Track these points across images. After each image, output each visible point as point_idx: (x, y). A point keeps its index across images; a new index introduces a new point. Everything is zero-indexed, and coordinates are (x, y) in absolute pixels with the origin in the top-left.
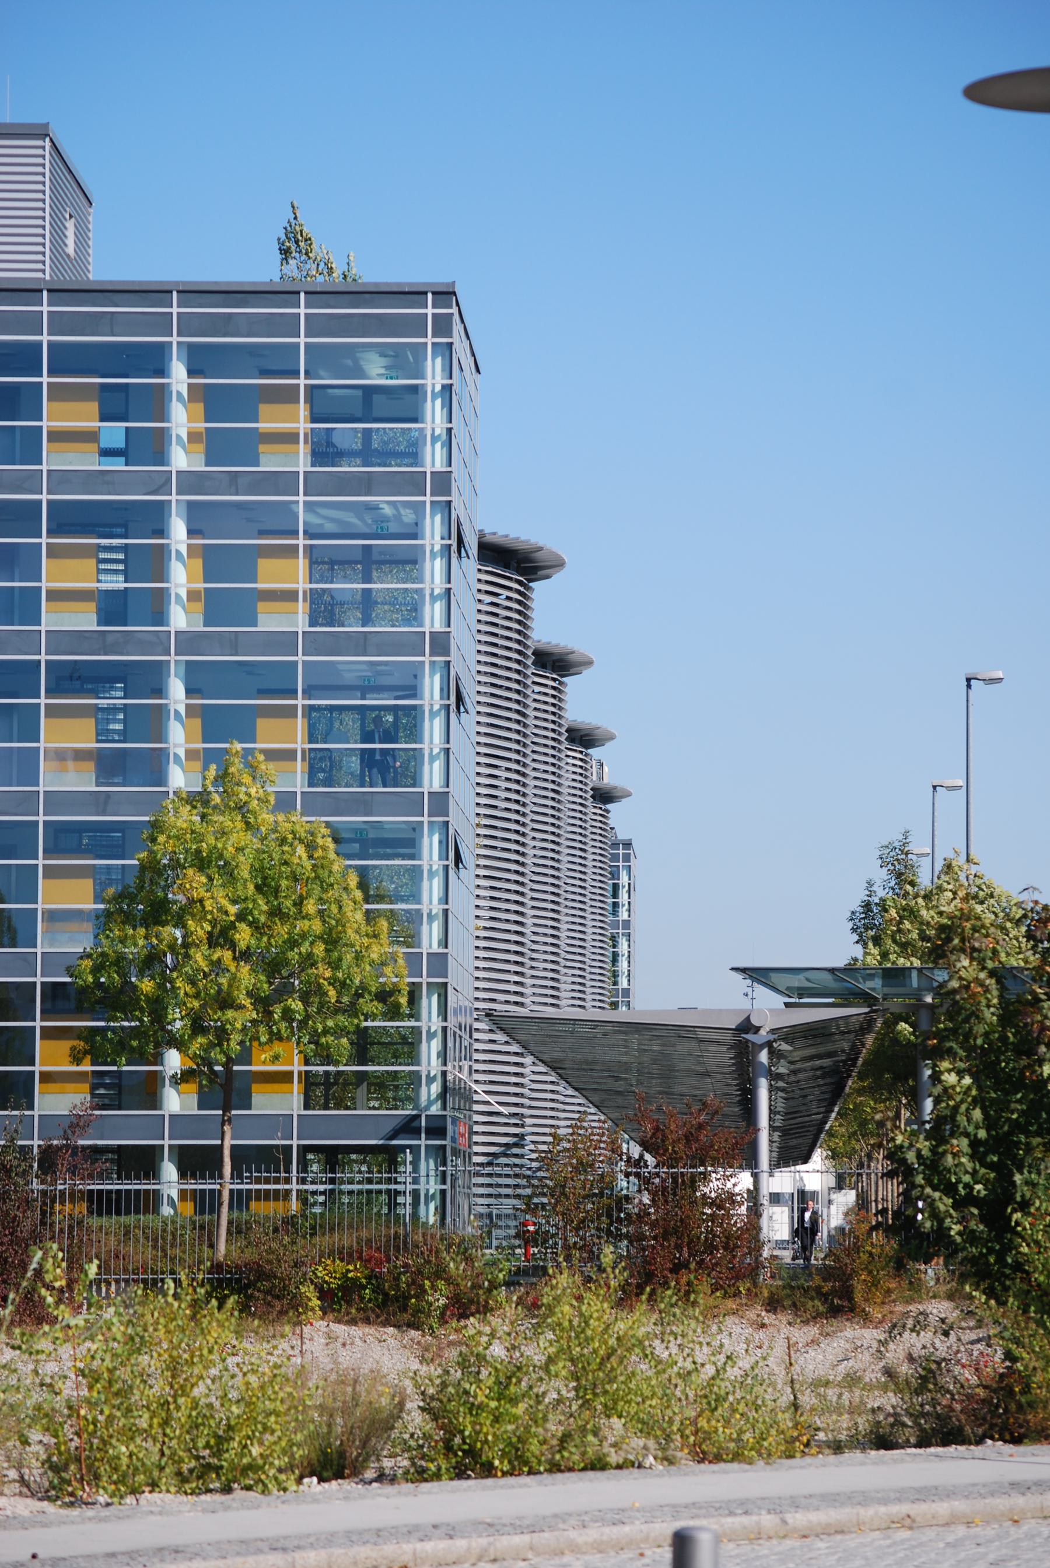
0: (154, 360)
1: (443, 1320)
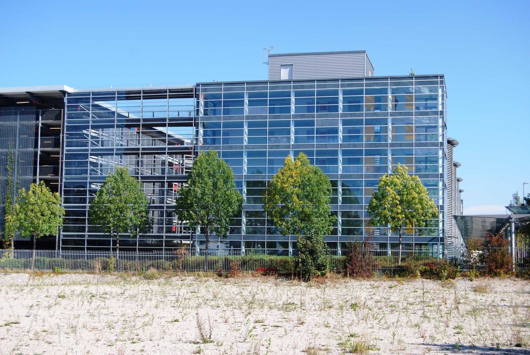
0: (385, 91)
1: (446, 279)
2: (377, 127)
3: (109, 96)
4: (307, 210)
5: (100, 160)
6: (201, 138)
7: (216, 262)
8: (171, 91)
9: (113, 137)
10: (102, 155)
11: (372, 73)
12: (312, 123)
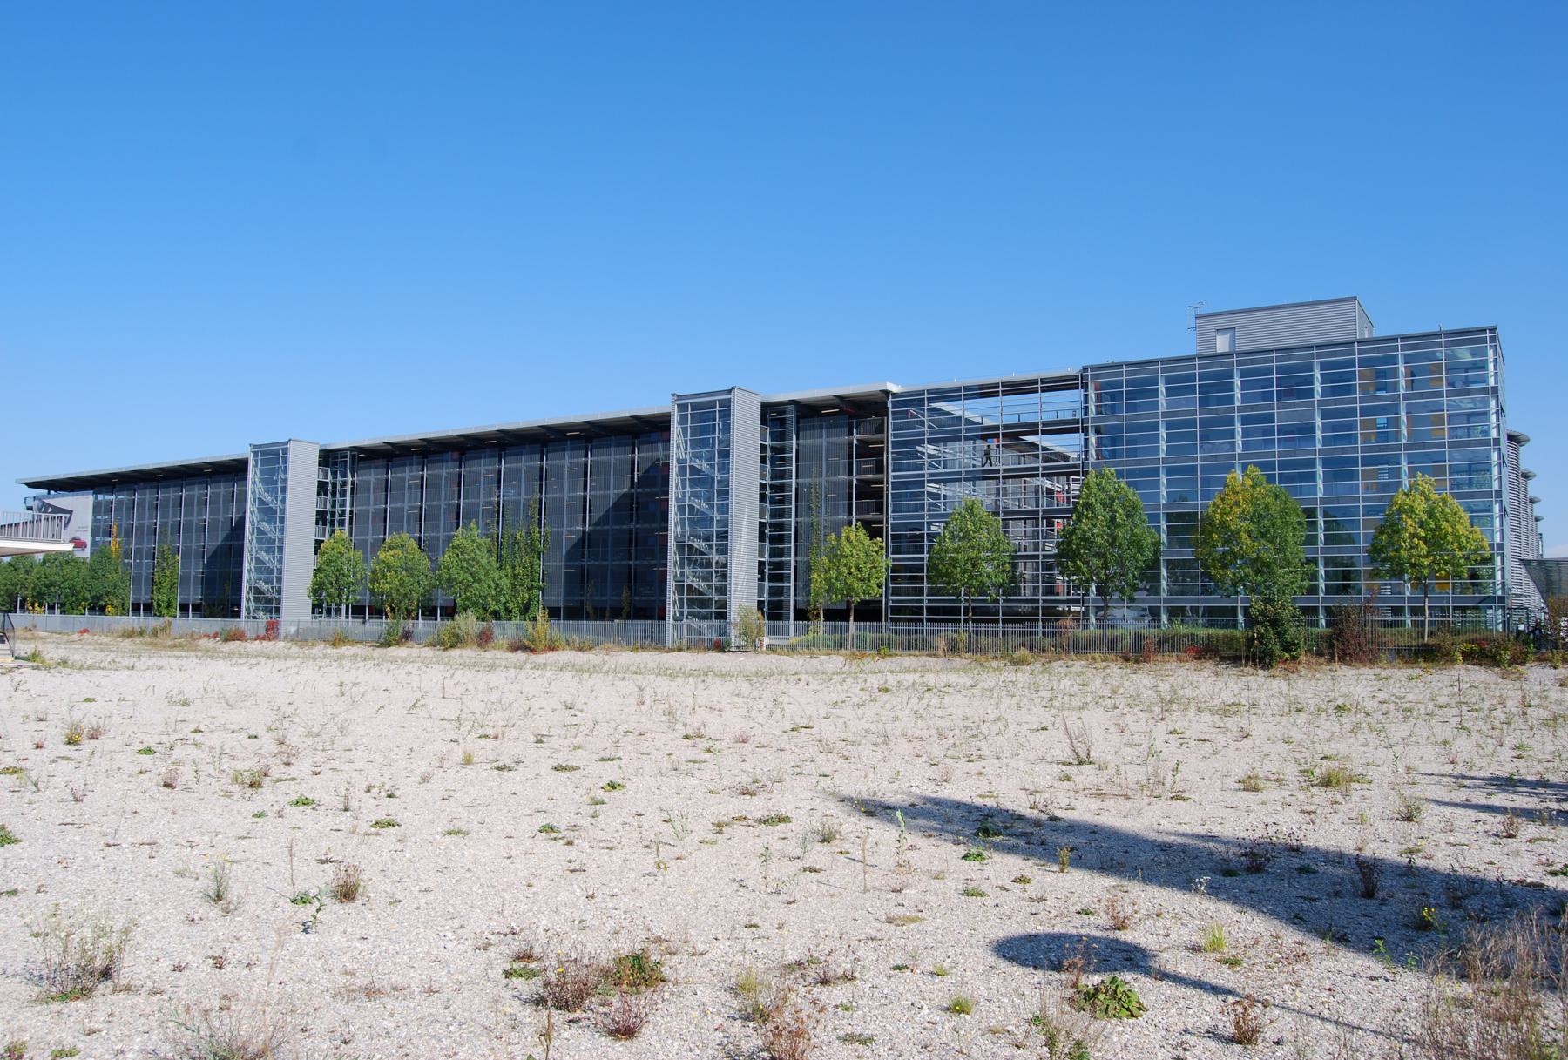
0: (1394, 360)
2: (1381, 420)
3: (952, 394)
4: (1264, 555)
5: (943, 490)
6: (1092, 451)
7: (1118, 639)
8: (966, 388)
9: (963, 455)
10: (945, 482)
11: (1370, 332)
12: (1270, 418)
